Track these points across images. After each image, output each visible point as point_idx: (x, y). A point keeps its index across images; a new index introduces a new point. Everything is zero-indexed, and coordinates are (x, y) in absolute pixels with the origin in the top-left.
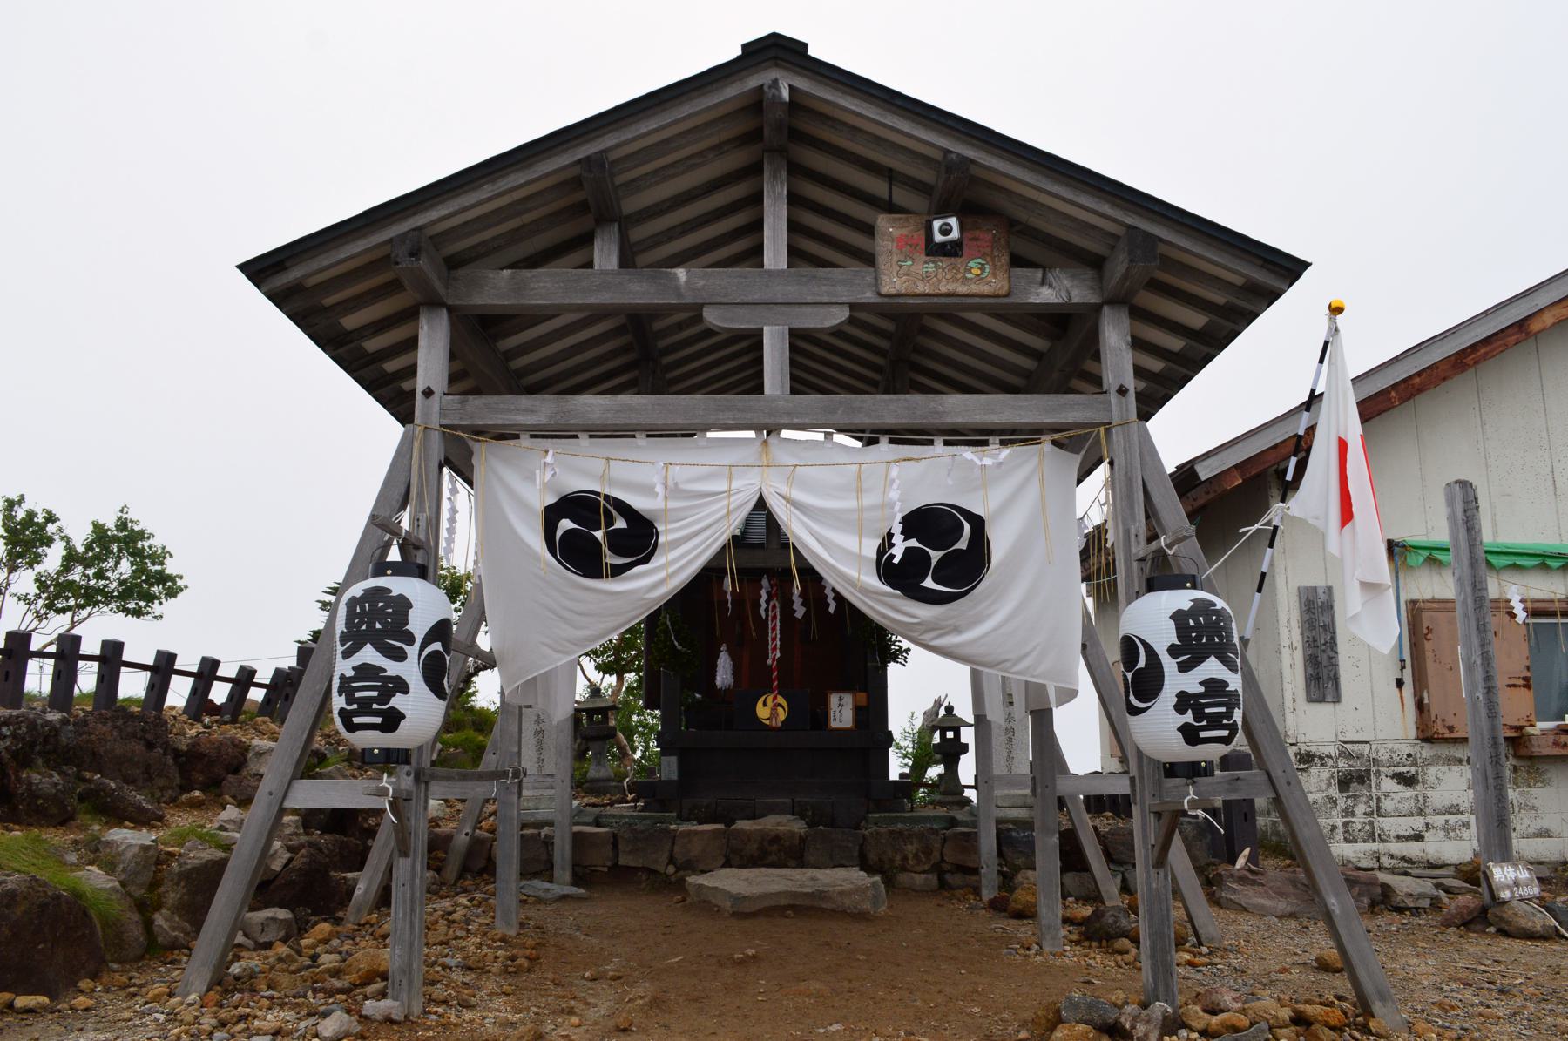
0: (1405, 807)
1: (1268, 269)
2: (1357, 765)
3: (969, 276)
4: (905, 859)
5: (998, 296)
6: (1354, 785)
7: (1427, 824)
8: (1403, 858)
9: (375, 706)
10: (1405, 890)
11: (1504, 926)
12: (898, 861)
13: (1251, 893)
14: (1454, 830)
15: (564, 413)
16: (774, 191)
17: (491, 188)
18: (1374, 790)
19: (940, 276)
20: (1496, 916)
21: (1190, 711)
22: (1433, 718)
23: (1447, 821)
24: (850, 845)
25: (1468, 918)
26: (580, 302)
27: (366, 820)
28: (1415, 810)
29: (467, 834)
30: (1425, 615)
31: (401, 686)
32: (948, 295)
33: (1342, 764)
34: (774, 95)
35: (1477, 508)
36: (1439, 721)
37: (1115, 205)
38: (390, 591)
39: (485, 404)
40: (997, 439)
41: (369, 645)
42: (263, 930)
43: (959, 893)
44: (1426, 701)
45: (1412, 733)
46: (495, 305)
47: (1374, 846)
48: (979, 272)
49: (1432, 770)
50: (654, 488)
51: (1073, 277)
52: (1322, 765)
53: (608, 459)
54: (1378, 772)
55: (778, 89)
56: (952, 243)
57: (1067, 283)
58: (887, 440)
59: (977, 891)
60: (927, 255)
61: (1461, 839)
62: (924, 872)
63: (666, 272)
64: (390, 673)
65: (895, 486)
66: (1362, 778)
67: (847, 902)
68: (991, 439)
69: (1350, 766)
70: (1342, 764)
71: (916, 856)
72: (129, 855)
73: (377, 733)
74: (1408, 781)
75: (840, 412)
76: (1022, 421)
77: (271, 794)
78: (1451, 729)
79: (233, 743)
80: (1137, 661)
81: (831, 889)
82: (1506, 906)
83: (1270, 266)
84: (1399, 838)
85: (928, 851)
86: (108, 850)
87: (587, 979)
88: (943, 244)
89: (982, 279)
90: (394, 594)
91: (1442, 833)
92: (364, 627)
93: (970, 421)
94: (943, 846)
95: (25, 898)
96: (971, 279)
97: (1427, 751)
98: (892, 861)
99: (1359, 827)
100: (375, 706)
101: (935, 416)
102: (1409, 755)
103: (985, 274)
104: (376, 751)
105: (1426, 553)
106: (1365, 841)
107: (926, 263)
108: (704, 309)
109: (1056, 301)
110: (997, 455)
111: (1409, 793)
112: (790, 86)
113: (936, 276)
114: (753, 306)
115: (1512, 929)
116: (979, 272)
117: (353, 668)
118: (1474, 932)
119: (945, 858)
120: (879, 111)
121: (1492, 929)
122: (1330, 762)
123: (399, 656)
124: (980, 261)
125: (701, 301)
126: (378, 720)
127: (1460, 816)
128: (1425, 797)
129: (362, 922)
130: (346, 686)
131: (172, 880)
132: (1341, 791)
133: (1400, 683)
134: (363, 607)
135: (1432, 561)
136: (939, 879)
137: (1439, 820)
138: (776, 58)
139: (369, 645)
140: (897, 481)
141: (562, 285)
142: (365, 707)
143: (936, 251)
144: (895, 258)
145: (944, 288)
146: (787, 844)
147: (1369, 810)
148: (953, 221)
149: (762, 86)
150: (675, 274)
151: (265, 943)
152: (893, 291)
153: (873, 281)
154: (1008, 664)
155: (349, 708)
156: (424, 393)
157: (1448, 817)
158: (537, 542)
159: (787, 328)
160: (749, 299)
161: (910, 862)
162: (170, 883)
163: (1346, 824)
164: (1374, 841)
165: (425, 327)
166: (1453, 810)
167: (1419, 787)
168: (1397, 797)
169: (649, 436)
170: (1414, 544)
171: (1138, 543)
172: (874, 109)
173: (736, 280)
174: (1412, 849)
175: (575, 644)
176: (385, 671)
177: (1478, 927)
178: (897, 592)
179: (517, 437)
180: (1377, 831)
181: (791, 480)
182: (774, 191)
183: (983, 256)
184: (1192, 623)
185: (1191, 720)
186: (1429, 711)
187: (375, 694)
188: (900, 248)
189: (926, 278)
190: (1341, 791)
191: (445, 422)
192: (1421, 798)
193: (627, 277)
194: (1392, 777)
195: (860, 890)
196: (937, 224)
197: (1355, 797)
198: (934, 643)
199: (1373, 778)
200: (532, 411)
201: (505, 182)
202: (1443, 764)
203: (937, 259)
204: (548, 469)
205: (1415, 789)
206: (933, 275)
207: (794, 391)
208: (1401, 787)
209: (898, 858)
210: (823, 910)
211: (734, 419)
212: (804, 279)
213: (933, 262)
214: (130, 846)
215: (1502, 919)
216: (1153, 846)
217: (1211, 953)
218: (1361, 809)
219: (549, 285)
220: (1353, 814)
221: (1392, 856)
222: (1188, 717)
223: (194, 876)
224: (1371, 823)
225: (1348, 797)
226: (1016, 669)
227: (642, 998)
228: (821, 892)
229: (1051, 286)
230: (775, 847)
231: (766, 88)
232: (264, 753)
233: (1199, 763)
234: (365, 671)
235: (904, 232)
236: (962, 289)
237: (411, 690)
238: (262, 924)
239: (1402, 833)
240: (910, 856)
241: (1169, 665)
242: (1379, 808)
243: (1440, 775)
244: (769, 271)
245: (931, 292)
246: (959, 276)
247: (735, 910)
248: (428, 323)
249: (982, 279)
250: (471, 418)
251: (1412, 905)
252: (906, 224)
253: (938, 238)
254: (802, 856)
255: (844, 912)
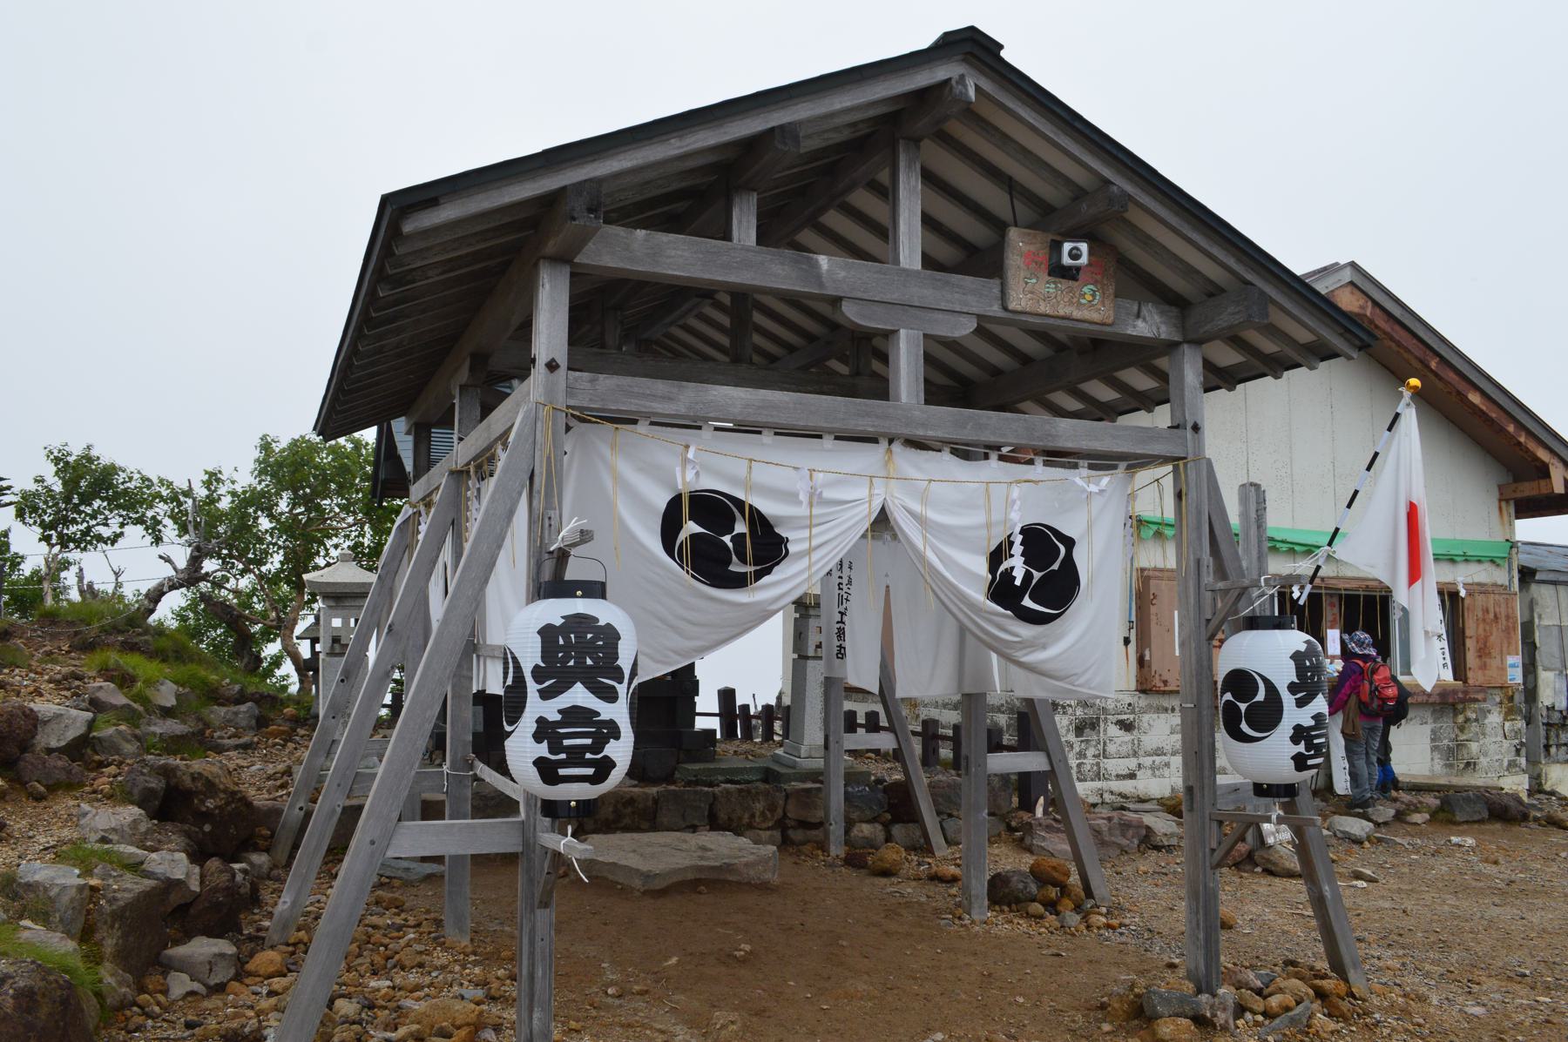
0: (1125, 749)
1: (1345, 339)
2: (1090, 713)
3: (1083, 301)
4: (753, 816)
5: (1104, 324)
6: (1087, 731)
7: (1139, 764)
8: (1120, 794)
9: (588, 756)
10: (1162, 831)
11: (1269, 866)
12: (746, 820)
13: (1057, 840)
14: (1158, 769)
15: (704, 404)
16: (909, 183)
17: (678, 144)
18: (1101, 735)
19: (1059, 299)
20: (1263, 858)
21: (1303, 742)
22: (1153, 673)
23: (1154, 762)
24: (702, 805)
25: (1239, 860)
26: (720, 279)
27: (203, 802)
28: (1131, 752)
29: (301, 809)
30: (1152, 582)
31: (613, 731)
32: (1063, 318)
33: (1079, 712)
34: (961, 92)
35: (1265, 509)
36: (1157, 676)
37: (1239, 260)
38: (597, 620)
39: (618, 386)
40: (1086, 463)
41: (579, 685)
42: (211, 970)
43: (807, 848)
44: (1147, 658)
45: (1133, 686)
46: (628, 270)
47: (1098, 784)
48: (1091, 298)
49: (1146, 718)
50: (798, 495)
51: (1162, 313)
52: (1064, 713)
53: (751, 460)
54: (1106, 719)
55: (965, 86)
56: (1078, 269)
57: (1157, 318)
58: (996, 457)
59: (823, 846)
60: (1049, 275)
61: (1163, 777)
62: (768, 829)
63: (808, 258)
64: (604, 717)
65: (1016, 507)
66: (1093, 724)
67: (752, 873)
68: (1081, 462)
69: (1085, 714)
70: (1079, 712)
71: (763, 813)
72: (65, 899)
73: (587, 785)
74: (1127, 726)
75: (969, 427)
76: (1119, 450)
77: (373, 843)
78: (1165, 682)
79: (24, 713)
80: (1256, 695)
81: (736, 861)
82: (1272, 850)
83: (1348, 336)
84: (1118, 777)
85: (772, 808)
86: (32, 896)
87: (612, 996)
88: (1070, 268)
89: (1093, 305)
90: (602, 623)
91: (1150, 772)
92: (571, 663)
93: (1077, 446)
94: (785, 804)
95: (44, 995)
96: (1084, 304)
97: (1143, 701)
98: (740, 819)
99: (1089, 768)
100: (588, 756)
101: (1050, 438)
102: (1130, 705)
103: (1096, 302)
104: (573, 804)
105: (1155, 527)
106: (1092, 780)
107: (1048, 283)
108: (843, 303)
109: (1149, 335)
110: (1080, 478)
111: (1127, 737)
112: (976, 85)
113: (1056, 297)
114: (890, 306)
115: (1278, 869)
116: (1091, 298)
117: (560, 712)
118: (1245, 871)
119: (789, 815)
120: (1055, 129)
121: (1259, 869)
122: (1070, 711)
123: (610, 696)
124: (1092, 287)
125: (843, 295)
126: (590, 771)
127: (1164, 757)
128: (1139, 741)
129: (292, 941)
130: (544, 730)
131: (105, 923)
132: (1077, 736)
133: (1127, 641)
134: (567, 639)
135: (1159, 535)
136: (783, 836)
137: (1147, 761)
138: (971, 54)
139: (579, 685)
140: (1018, 503)
141: (701, 256)
142: (576, 755)
143: (1061, 272)
144: (1022, 275)
145: (1063, 310)
146: (640, 806)
147: (1097, 752)
148: (1084, 247)
149: (950, 79)
150: (817, 261)
151: (217, 985)
152: (1019, 308)
153: (999, 295)
154: (1075, 678)
155: (553, 757)
156: (558, 366)
157: (1155, 758)
158: (655, 545)
159: (921, 333)
160: (888, 297)
161: (757, 820)
162: (105, 927)
163: (1079, 765)
164: (1099, 780)
165: (547, 286)
166: (1159, 752)
167: (1136, 731)
168: (1118, 741)
169: (776, 434)
170: (1147, 519)
171: (1208, 573)
172: (1049, 126)
173: (875, 276)
174: (1127, 786)
175: (679, 655)
176: (598, 714)
177: (1248, 867)
178: (1009, 612)
179: (635, 422)
180: (1102, 771)
181: (924, 499)
182: (909, 183)
183: (1095, 283)
184: (1308, 664)
185: (1303, 751)
186: (1150, 667)
187: (588, 741)
188: (1028, 265)
189: (1047, 298)
190: (1077, 736)
191: (572, 402)
192: (1136, 742)
193: (769, 257)
194: (1116, 724)
195: (764, 861)
196: (1067, 246)
197: (1087, 741)
198: (1023, 659)
199: (1102, 724)
200: (670, 399)
201: (693, 139)
202: (1154, 713)
203: (1057, 280)
204: (689, 467)
205: (1132, 734)
206: (1053, 296)
207: (927, 402)
208: (1122, 732)
209: (746, 816)
210: (730, 883)
211: (873, 426)
212: (939, 283)
213: (1054, 283)
214: (64, 888)
215: (1268, 861)
216: (1213, 850)
217: (1108, 912)
218: (1091, 752)
219: (686, 254)
220: (1085, 756)
221: (1112, 793)
222: (1301, 748)
223: (127, 914)
224: (1098, 764)
225: (1082, 741)
226: (1082, 680)
227: (732, 1022)
228: (728, 865)
229: (1144, 319)
230: (629, 810)
231: (953, 82)
232: (49, 721)
233: (1262, 784)
234: (575, 715)
235: (1032, 248)
236: (1077, 314)
237: (621, 739)
238: (210, 962)
239: (1121, 772)
240: (758, 814)
241: (1288, 700)
242: (1104, 750)
243: (1151, 722)
244: (905, 270)
245: (1051, 313)
246: (1075, 300)
247: (646, 888)
248: (550, 281)
249: (1093, 305)
250: (602, 400)
251: (1166, 843)
252: (1034, 241)
253: (1066, 260)
254: (655, 818)
255: (749, 883)
